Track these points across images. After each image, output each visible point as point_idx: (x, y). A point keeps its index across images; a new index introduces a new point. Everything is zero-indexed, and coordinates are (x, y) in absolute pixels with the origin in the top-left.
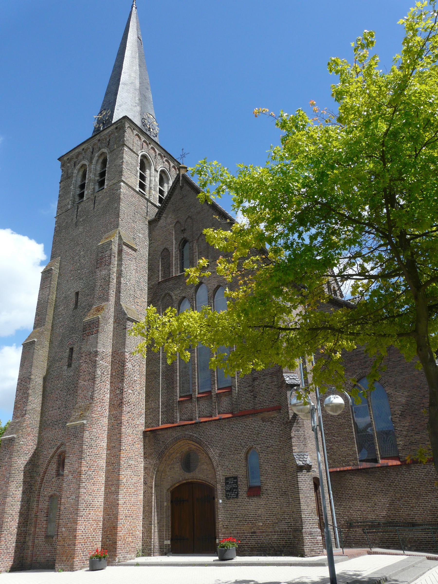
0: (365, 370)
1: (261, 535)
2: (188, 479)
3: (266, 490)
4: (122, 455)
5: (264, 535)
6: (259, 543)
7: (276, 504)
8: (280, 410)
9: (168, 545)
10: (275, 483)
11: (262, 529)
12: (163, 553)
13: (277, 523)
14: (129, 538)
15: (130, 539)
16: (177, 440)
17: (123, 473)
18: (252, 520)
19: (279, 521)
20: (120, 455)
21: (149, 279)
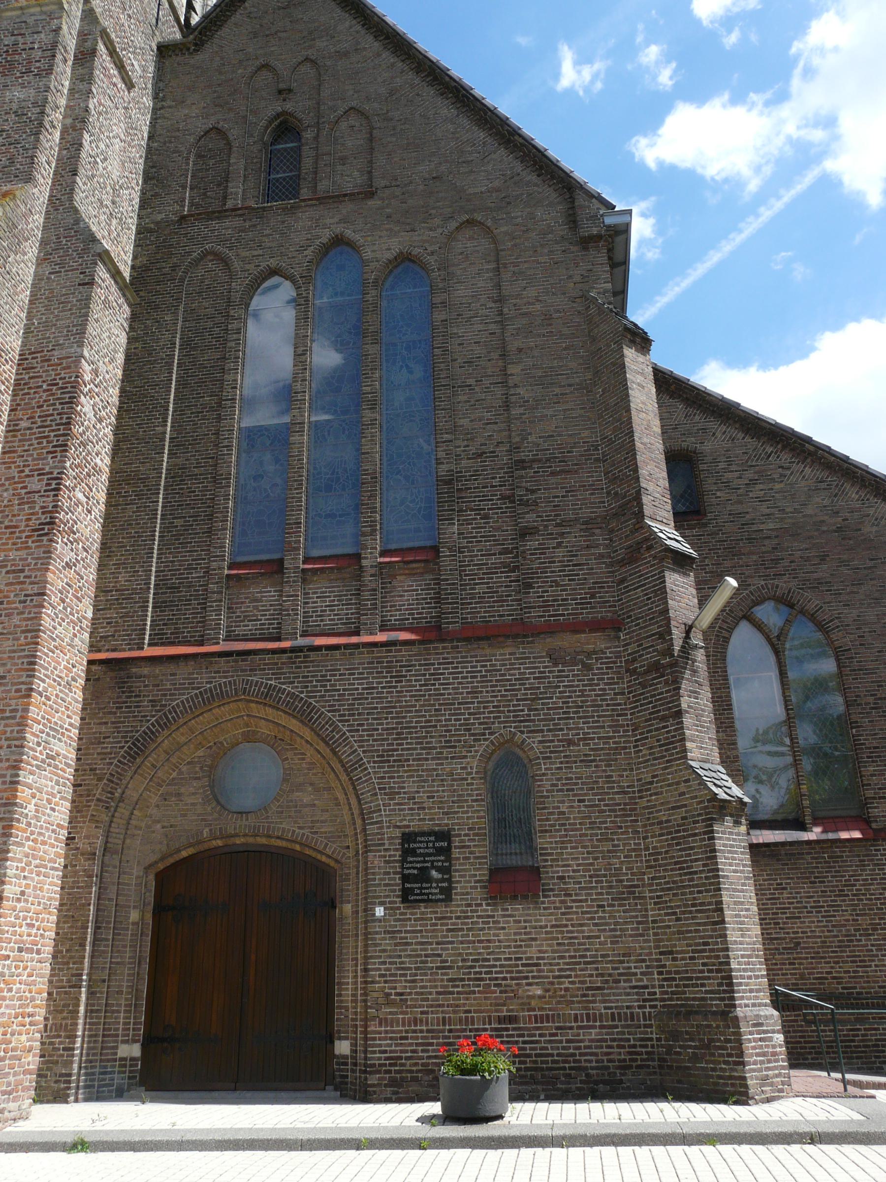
0: (776, 582)
1: (538, 1028)
2: (236, 835)
3: (562, 878)
4: (33, 712)
5: (547, 1028)
6: (529, 1056)
7: (596, 925)
8: (620, 630)
9: (133, 1059)
10: (596, 859)
11: (541, 1009)
12: (99, 1091)
13: (598, 988)
14: (20, 1034)
15: (24, 1038)
16: (211, 698)
17: (30, 779)
18: (505, 979)
19: (607, 982)
20: (26, 710)
21: (144, 203)
